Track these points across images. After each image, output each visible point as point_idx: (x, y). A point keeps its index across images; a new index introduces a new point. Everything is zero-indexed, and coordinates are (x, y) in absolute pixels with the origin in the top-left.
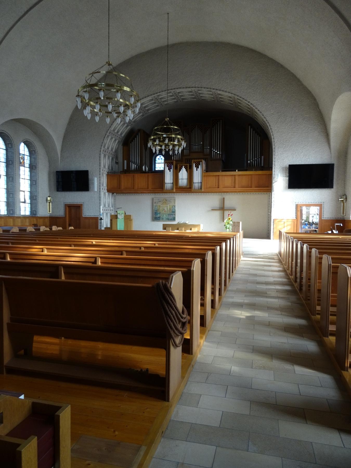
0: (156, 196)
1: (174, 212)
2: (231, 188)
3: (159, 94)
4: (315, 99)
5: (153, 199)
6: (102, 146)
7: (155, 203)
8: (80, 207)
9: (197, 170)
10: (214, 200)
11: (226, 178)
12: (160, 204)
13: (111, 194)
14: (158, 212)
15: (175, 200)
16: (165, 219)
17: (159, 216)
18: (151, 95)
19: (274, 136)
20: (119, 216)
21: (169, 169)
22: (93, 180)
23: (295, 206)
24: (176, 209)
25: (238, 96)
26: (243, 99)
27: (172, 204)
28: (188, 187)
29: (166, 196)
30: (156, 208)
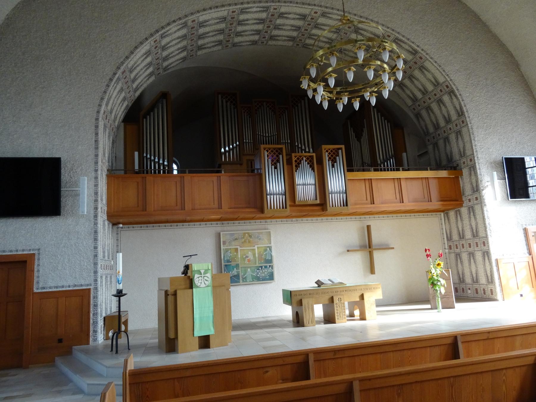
0: (225, 228)
2: (395, 203)
3: (246, 6)
4: (512, 56)
5: (219, 236)
6: (102, 99)
7: (224, 243)
8: (25, 262)
10: (348, 230)
11: (383, 184)
13: (111, 225)
14: (233, 264)
16: (249, 279)
17: (235, 272)
18: (230, 5)
19: (468, 107)
20: (197, 280)
21: (357, 140)
22: (76, 184)
23: (522, 232)
24: (274, 254)
25: (398, 33)
26: (408, 39)
27: (263, 244)
28: (318, 202)
29: (249, 227)
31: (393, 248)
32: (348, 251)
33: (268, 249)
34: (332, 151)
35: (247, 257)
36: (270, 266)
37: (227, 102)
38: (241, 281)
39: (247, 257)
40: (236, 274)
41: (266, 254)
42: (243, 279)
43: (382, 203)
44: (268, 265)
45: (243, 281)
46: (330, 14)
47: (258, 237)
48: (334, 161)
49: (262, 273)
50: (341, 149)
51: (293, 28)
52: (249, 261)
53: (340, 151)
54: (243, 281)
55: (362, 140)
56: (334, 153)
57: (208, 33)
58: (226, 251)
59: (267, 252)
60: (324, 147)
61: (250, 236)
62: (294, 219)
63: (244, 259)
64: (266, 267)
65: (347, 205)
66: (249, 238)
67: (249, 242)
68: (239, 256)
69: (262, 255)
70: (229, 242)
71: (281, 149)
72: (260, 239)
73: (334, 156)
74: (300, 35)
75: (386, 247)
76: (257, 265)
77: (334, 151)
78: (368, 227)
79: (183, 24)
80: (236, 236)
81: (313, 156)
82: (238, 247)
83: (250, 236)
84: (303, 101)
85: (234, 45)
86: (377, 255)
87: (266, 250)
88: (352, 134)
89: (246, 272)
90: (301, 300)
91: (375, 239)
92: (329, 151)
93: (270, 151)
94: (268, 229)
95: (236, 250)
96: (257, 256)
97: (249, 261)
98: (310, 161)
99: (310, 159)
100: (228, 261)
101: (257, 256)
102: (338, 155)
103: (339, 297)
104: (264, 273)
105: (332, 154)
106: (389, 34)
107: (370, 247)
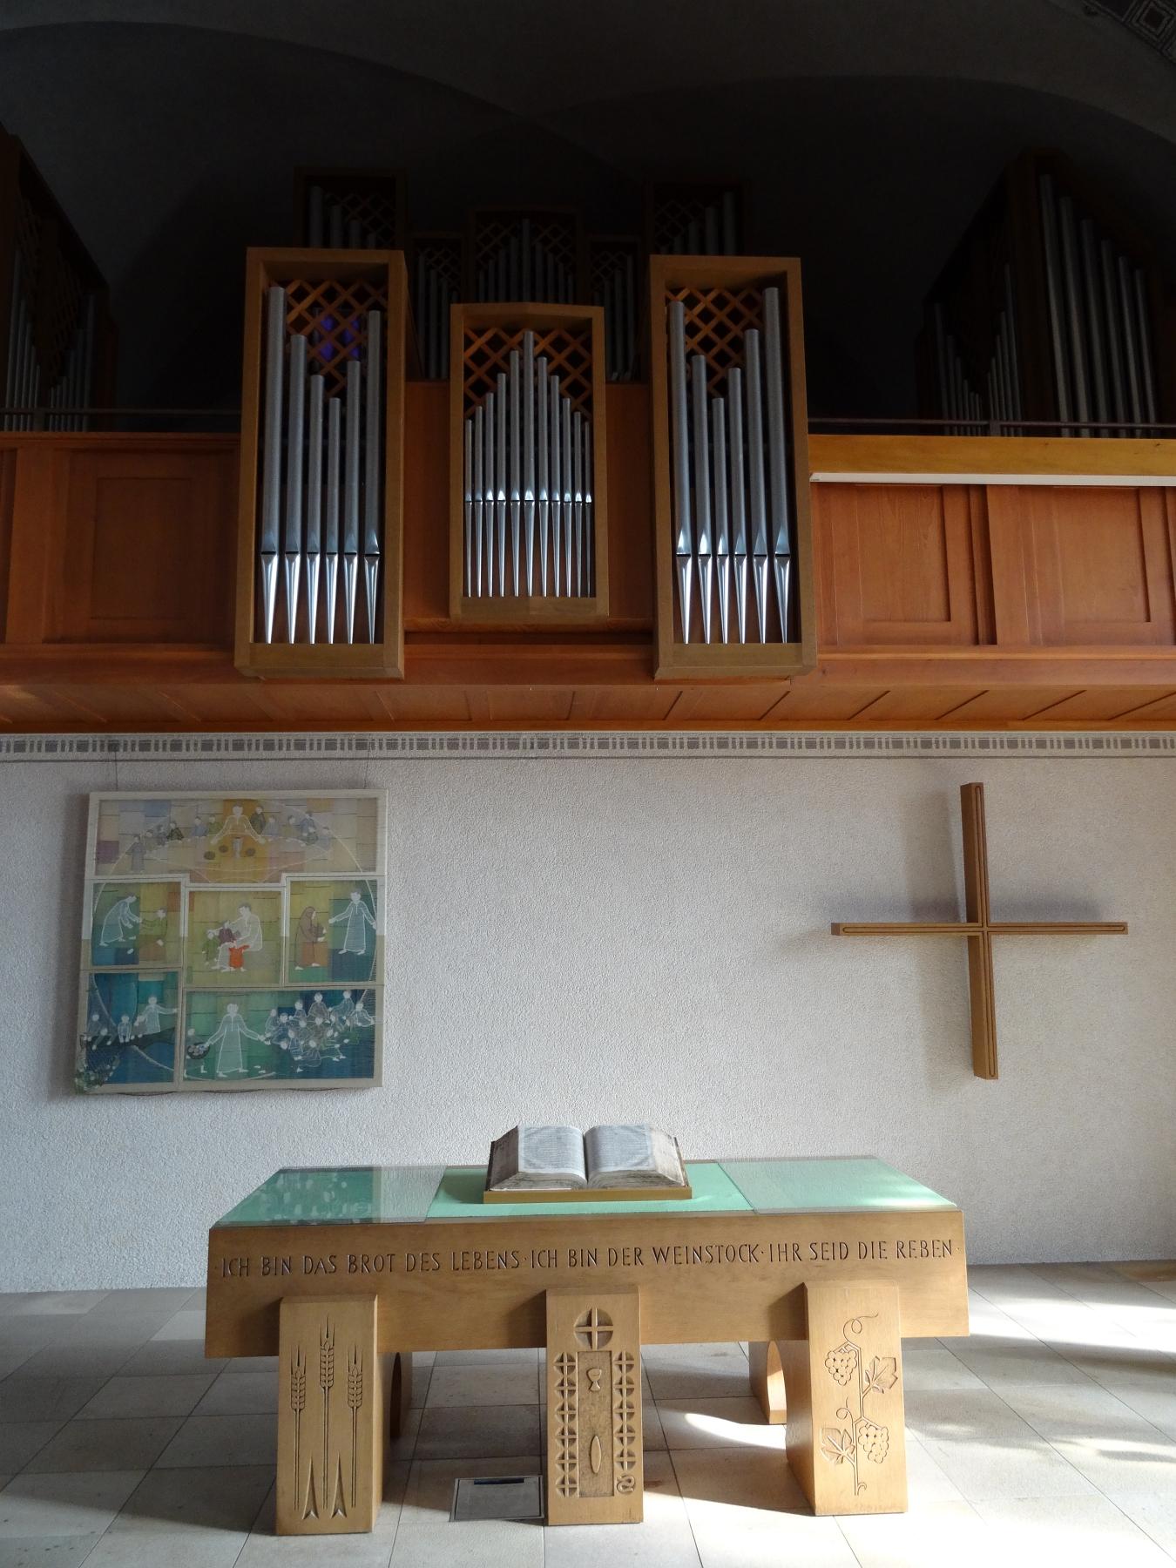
0: (126, 773)
1: (357, 969)
2: (1137, 641)
5: (78, 809)
9: (720, 388)
10: (849, 811)
12: (164, 865)
15: (369, 813)
16: (230, 1061)
17: (150, 1018)
24: (389, 926)
27: (331, 865)
28: (602, 607)
30: (123, 915)
31: (1120, 928)
32: (836, 929)
33: (356, 897)
35: (227, 935)
36: (356, 994)
38: (180, 1071)
39: (227, 935)
40: (154, 1028)
41: (341, 926)
42: (195, 1058)
43: (1051, 642)
44: (346, 987)
45: (194, 1074)
47: (301, 827)
48: (724, 355)
49: (303, 1035)
50: (779, 281)
52: (237, 959)
53: (772, 294)
54: (194, 1074)
58: (116, 893)
59: (348, 913)
60: (663, 267)
61: (258, 822)
62: (526, 735)
63: (210, 949)
64: (332, 998)
65: (795, 635)
66: (249, 831)
67: (250, 853)
68: (184, 931)
69: (317, 931)
70: (132, 851)
71: (379, 278)
72: (312, 839)
73: (735, 330)
75: (1072, 921)
76: (284, 983)
77: (735, 302)
78: (971, 796)
80: (177, 817)
82: (184, 879)
83: (258, 822)
86: (1012, 963)
87: (341, 903)
89: (216, 1015)
90: (272, 1312)
91: (1012, 865)
94: (365, 786)
95: (173, 890)
96: (285, 931)
97: (237, 959)
98: (575, 359)
100: (121, 956)
101: (285, 931)
102: (760, 322)
103: (597, 1303)
104: (319, 1032)
105: (721, 316)
107: (972, 917)
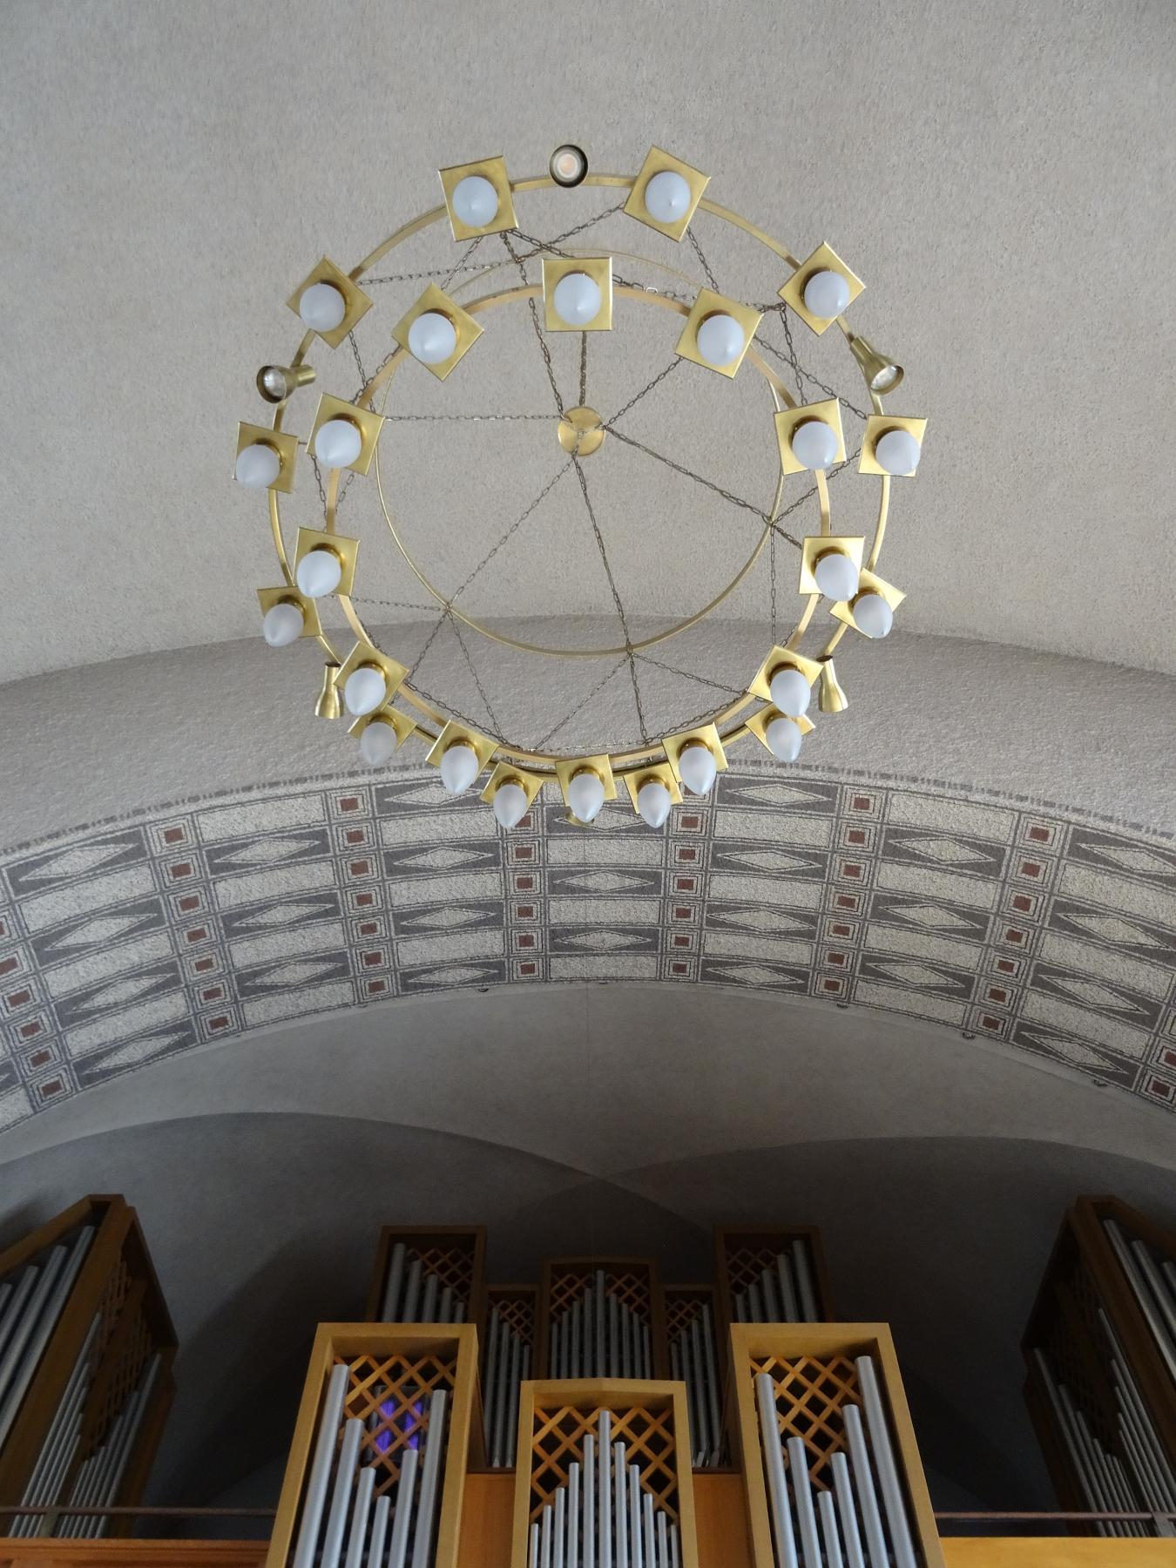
21: (1106, 1450)
34: (810, 1373)
37: (441, 1287)
46: (749, 783)
50: (870, 1348)
51: (627, 882)
53: (865, 1364)
55: (1126, 1437)
56: (829, 1389)
57: (265, 906)
60: (745, 1336)
73: (831, 1405)
74: (671, 915)
77: (827, 1373)
79: (123, 839)
81: (669, 1400)
84: (782, 1260)
85: (410, 981)
88: (1075, 1426)
92: (794, 1373)
93: (379, 1372)
99: (655, 1426)
105: (813, 1389)
106: (1036, 823)
